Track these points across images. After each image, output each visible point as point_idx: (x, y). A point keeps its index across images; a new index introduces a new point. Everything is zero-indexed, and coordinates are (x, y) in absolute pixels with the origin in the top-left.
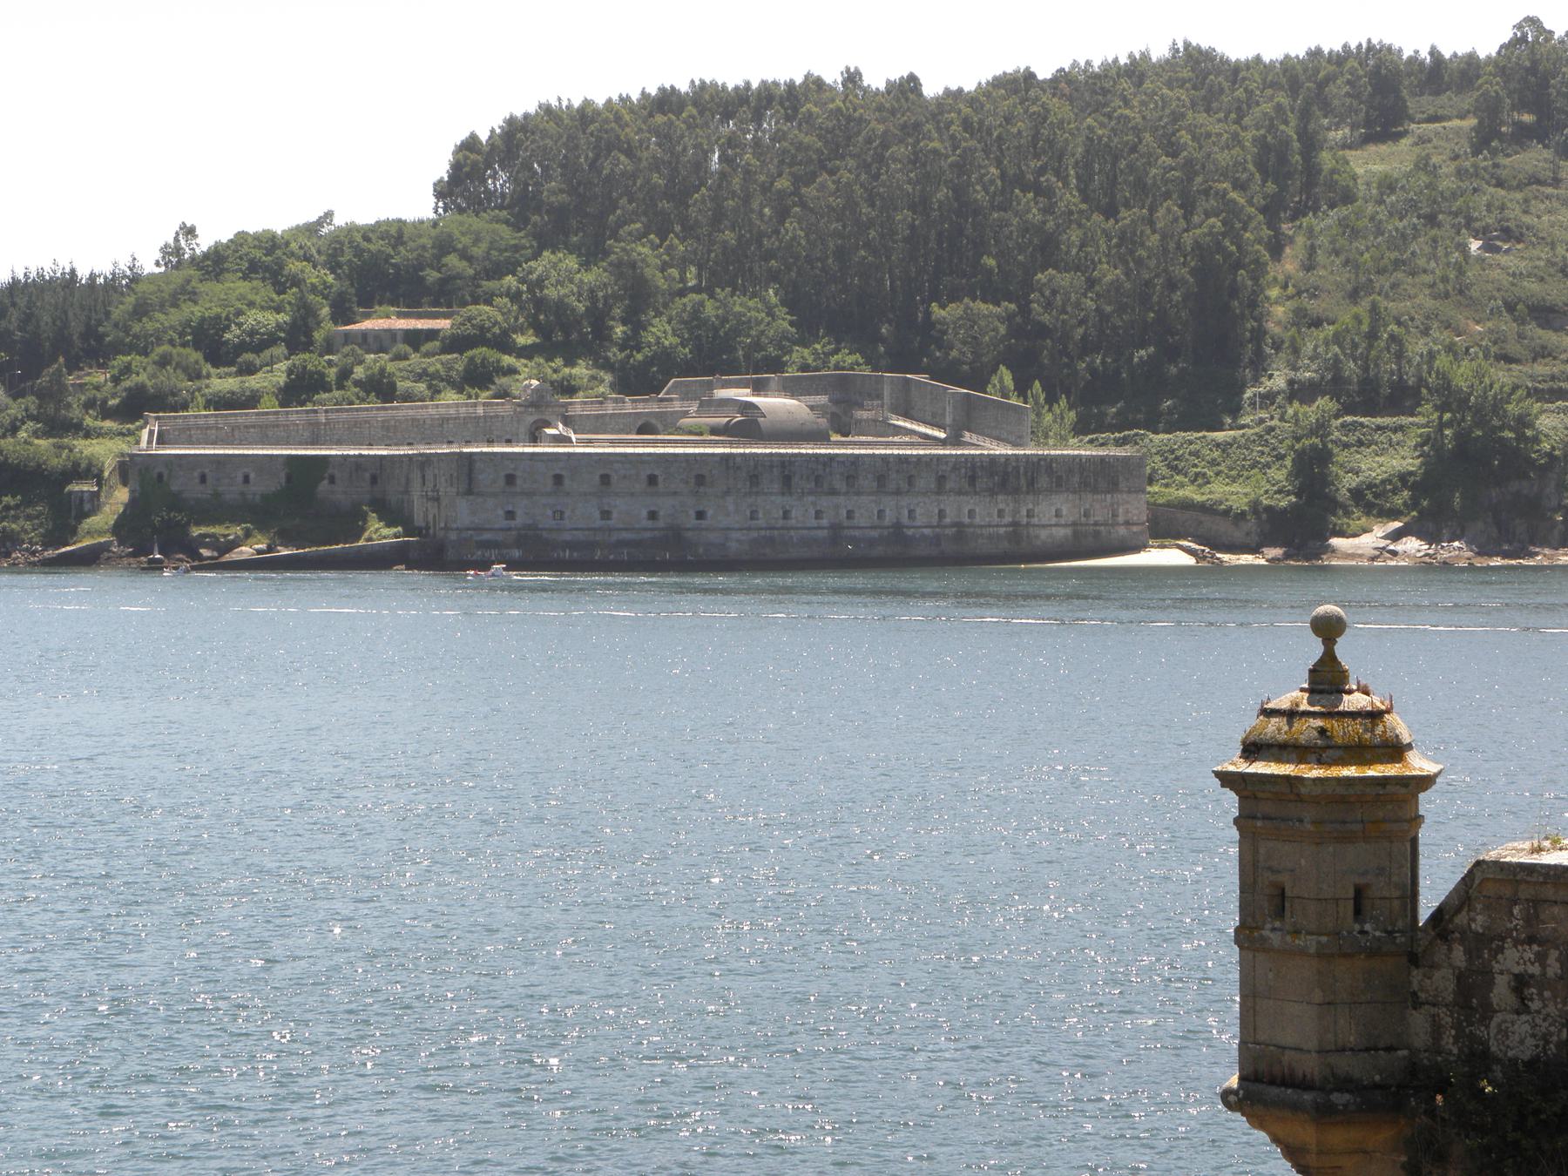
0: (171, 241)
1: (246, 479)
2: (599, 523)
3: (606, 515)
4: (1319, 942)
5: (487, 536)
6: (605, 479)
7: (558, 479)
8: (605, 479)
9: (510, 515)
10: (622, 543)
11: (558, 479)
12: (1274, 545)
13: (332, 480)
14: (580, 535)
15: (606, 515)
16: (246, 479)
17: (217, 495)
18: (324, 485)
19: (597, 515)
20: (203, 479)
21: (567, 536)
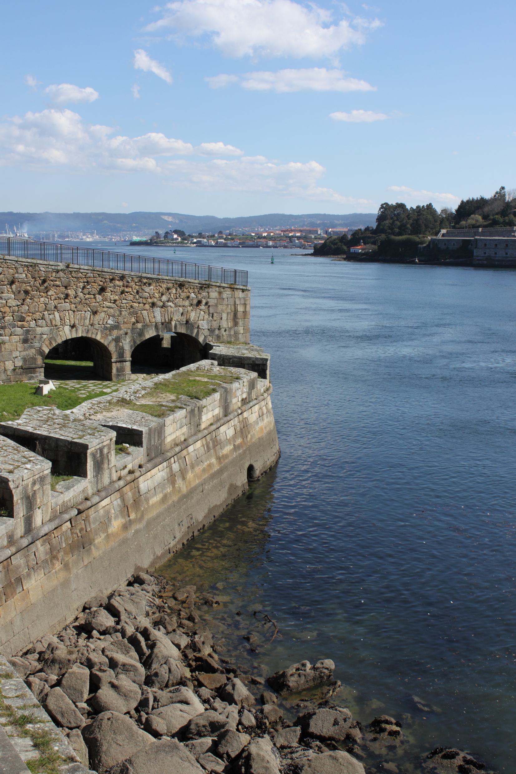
0: (499, 190)
1: (454, 245)
2: (505, 255)
3: (507, 254)
4: (212, 740)
5: (479, 258)
6: (507, 245)
7: (496, 245)
8: (507, 245)
9: (485, 253)
10: (509, 260)
11: (496, 245)
12: (395, 719)
13: (472, 245)
14: (500, 258)
15: (507, 254)
16: (454, 245)
17: (448, 248)
18: (470, 246)
19: (504, 253)
20: (445, 244)
21: (497, 258)
